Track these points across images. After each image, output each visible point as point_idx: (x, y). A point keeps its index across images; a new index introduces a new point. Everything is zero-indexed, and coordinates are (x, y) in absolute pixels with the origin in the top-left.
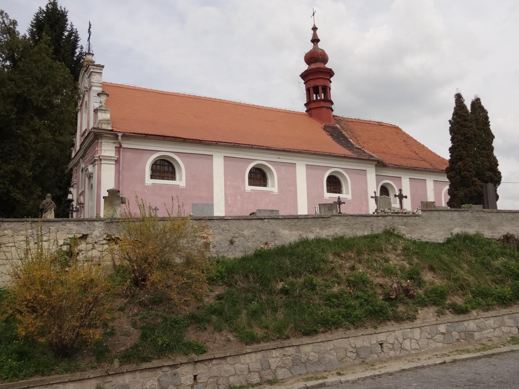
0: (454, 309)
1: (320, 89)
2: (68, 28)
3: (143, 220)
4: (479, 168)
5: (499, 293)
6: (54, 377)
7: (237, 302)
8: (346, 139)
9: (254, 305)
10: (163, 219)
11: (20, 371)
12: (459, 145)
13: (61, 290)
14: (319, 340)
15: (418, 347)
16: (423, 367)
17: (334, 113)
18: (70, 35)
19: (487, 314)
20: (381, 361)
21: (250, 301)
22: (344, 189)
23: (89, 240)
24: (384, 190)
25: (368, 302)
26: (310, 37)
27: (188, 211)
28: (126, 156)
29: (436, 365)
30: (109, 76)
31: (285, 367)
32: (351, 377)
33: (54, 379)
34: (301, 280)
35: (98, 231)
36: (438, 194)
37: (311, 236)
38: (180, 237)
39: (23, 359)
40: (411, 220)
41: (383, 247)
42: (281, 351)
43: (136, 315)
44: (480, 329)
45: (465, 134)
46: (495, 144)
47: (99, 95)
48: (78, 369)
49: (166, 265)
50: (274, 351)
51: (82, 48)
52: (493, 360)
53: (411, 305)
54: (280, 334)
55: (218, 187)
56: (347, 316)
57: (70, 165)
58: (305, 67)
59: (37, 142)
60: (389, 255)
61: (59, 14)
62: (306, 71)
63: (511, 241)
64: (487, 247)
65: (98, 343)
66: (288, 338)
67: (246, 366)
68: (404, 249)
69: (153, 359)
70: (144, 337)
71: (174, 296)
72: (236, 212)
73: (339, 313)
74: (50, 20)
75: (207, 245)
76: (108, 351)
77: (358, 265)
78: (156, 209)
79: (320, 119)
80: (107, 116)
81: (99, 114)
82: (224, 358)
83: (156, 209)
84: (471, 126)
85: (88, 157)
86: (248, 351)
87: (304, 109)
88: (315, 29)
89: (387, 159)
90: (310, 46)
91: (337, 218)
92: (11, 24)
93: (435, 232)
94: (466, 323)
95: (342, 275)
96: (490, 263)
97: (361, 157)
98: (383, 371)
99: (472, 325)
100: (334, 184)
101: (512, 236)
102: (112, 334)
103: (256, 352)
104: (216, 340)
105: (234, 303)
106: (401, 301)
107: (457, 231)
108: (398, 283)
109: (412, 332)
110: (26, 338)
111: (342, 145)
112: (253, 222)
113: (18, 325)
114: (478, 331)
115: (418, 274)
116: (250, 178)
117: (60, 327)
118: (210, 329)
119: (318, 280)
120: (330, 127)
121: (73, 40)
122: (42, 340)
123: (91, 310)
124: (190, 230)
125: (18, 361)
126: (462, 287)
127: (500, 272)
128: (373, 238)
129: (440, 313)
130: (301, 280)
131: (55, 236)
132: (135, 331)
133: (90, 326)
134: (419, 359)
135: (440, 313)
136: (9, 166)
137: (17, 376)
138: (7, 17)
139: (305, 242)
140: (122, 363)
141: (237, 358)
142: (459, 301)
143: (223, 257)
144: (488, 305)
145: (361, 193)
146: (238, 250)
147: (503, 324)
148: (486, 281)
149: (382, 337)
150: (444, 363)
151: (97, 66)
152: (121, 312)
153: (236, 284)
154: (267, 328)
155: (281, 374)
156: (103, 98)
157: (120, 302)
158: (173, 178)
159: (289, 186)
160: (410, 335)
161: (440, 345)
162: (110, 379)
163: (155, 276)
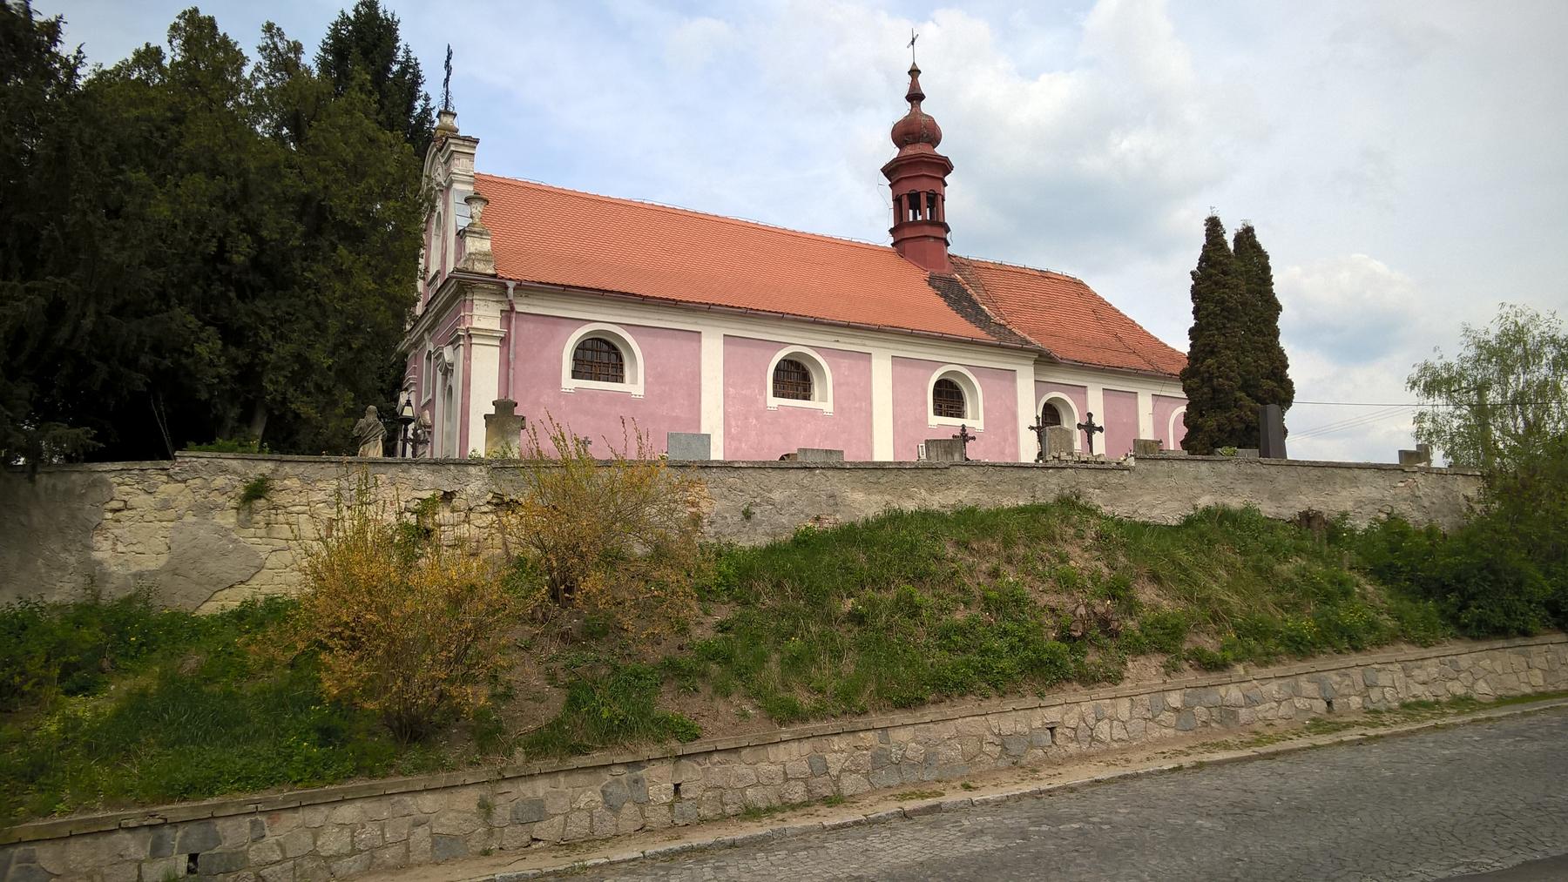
0: (1198, 660)
1: (923, 198)
2: (400, 55)
3: (565, 465)
4: (1249, 373)
5: (1289, 629)
6: (393, 780)
7: (760, 637)
8: (974, 304)
9: (795, 644)
10: (607, 464)
11: (327, 766)
12: (1209, 324)
13: (409, 604)
14: (927, 719)
15: (1125, 737)
16: (1137, 776)
17: (951, 250)
18: (404, 71)
19: (1265, 672)
20: (1051, 763)
21: (788, 636)
22: (968, 408)
23: (456, 502)
24: (1051, 414)
25: (1027, 644)
26: (905, 90)
27: (658, 449)
28: (524, 331)
29: (1162, 772)
30: (486, 162)
31: (857, 772)
32: (992, 794)
33: (394, 785)
34: (889, 596)
35: (475, 486)
36: (1160, 424)
37: (910, 506)
38: (645, 501)
39: (331, 743)
40: (1113, 478)
41: (1057, 531)
42: (850, 738)
43: (554, 659)
44: (1251, 702)
45: (1223, 301)
46: (1281, 323)
47: (468, 200)
48: (441, 765)
49: (613, 559)
50: (836, 739)
51: (427, 99)
52: (1279, 765)
53: (1113, 651)
54: (847, 704)
55: (712, 395)
56: (983, 671)
57: (403, 346)
58: (894, 152)
59: (345, 298)
60: (1068, 548)
61: (380, 26)
62: (895, 161)
63: (1315, 524)
64: (1267, 536)
65: (481, 715)
66: (864, 712)
67: (780, 767)
68: (1100, 536)
69: (593, 748)
70: (573, 703)
71: (628, 623)
72: (747, 452)
73: (968, 664)
74: (362, 39)
75: (696, 520)
76: (500, 730)
77: (1006, 569)
78: (586, 442)
79: (920, 260)
80: (485, 245)
81: (468, 240)
82: (736, 750)
83: (586, 442)
84: (1233, 281)
85: (443, 330)
86: (785, 737)
87: (888, 241)
88: (914, 72)
89: (1058, 349)
90: (905, 109)
91: (963, 470)
92: (290, 50)
93: (1162, 503)
94: (1222, 690)
95: (974, 588)
96: (1272, 568)
97: (1007, 344)
98: (1057, 783)
99: (1234, 694)
100: (949, 397)
101: (1318, 515)
102: (507, 696)
103: (799, 740)
104: (720, 714)
105: (755, 640)
106: (1093, 642)
107: (1205, 501)
108: (1087, 606)
109: (1114, 706)
110: (337, 702)
111: (966, 316)
112: (792, 476)
113: (323, 674)
114: (1246, 706)
115: (1128, 588)
116: (776, 381)
117: (407, 680)
118: (706, 690)
119: (923, 596)
120: (941, 278)
121: (410, 80)
122: (371, 705)
123: (467, 647)
124: (662, 487)
125: (321, 746)
126: (1215, 618)
127: (1293, 588)
128: (1035, 512)
129: (1171, 669)
130: (889, 596)
131: (394, 496)
132: (555, 692)
133: (467, 679)
134: (1128, 761)
135: (1171, 669)
136: (288, 347)
137: (321, 778)
138: (281, 35)
139: (895, 518)
140: (530, 756)
141: (761, 752)
142: (1210, 644)
143: (730, 545)
144: (1268, 654)
145: (1005, 419)
146: (760, 530)
147: (1296, 692)
148: (1264, 605)
149: (1053, 715)
150: (1180, 768)
151: (464, 139)
152: (524, 653)
153: (757, 600)
154: (821, 690)
155: (849, 784)
156: (477, 208)
157: (521, 633)
158: (619, 378)
159: (857, 401)
160: (1109, 712)
161: (1170, 732)
162: (506, 787)
163: (593, 582)
